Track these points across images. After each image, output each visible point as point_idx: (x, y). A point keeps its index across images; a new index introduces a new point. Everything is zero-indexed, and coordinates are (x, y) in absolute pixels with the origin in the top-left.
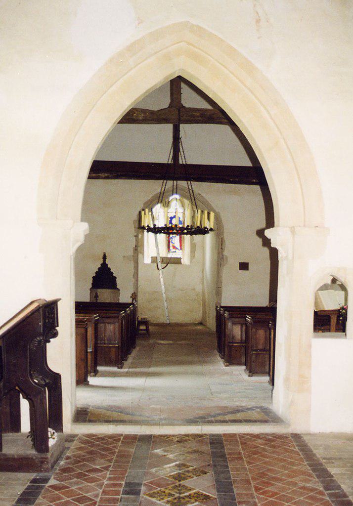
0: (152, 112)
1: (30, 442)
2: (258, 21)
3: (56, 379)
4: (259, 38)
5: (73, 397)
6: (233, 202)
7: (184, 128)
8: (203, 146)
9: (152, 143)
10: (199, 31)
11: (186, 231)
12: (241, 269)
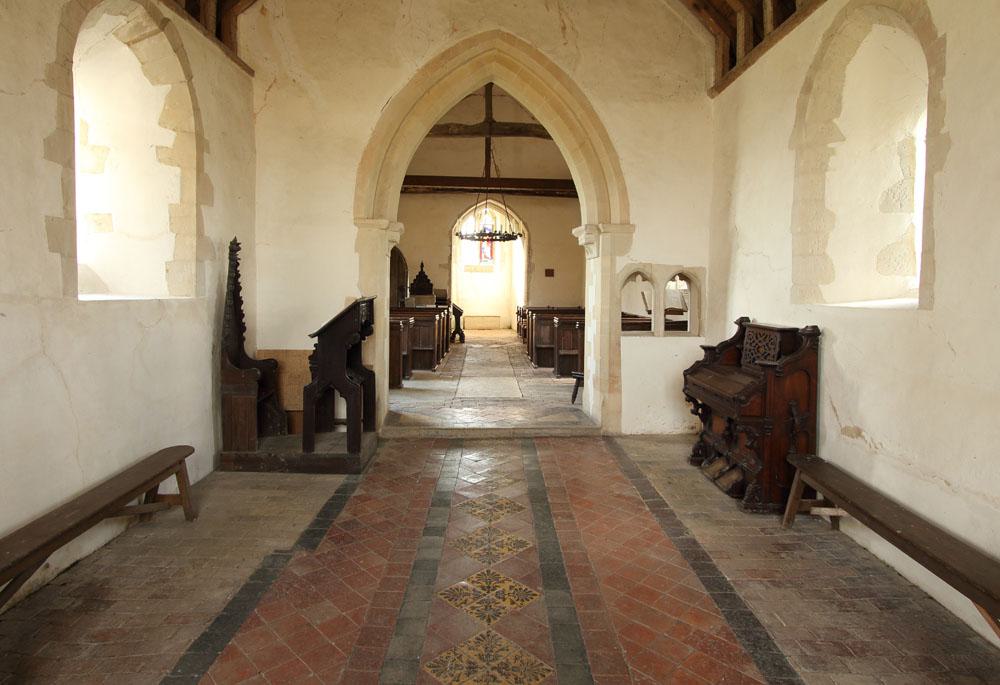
0: (466, 127)
1: (345, 441)
2: (564, 28)
3: (369, 376)
4: (565, 44)
5: (389, 401)
6: (546, 209)
7: (495, 140)
8: (513, 158)
9: (466, 158)
10: (510, 39)
11: (498, 237)
12: (553, 270)
